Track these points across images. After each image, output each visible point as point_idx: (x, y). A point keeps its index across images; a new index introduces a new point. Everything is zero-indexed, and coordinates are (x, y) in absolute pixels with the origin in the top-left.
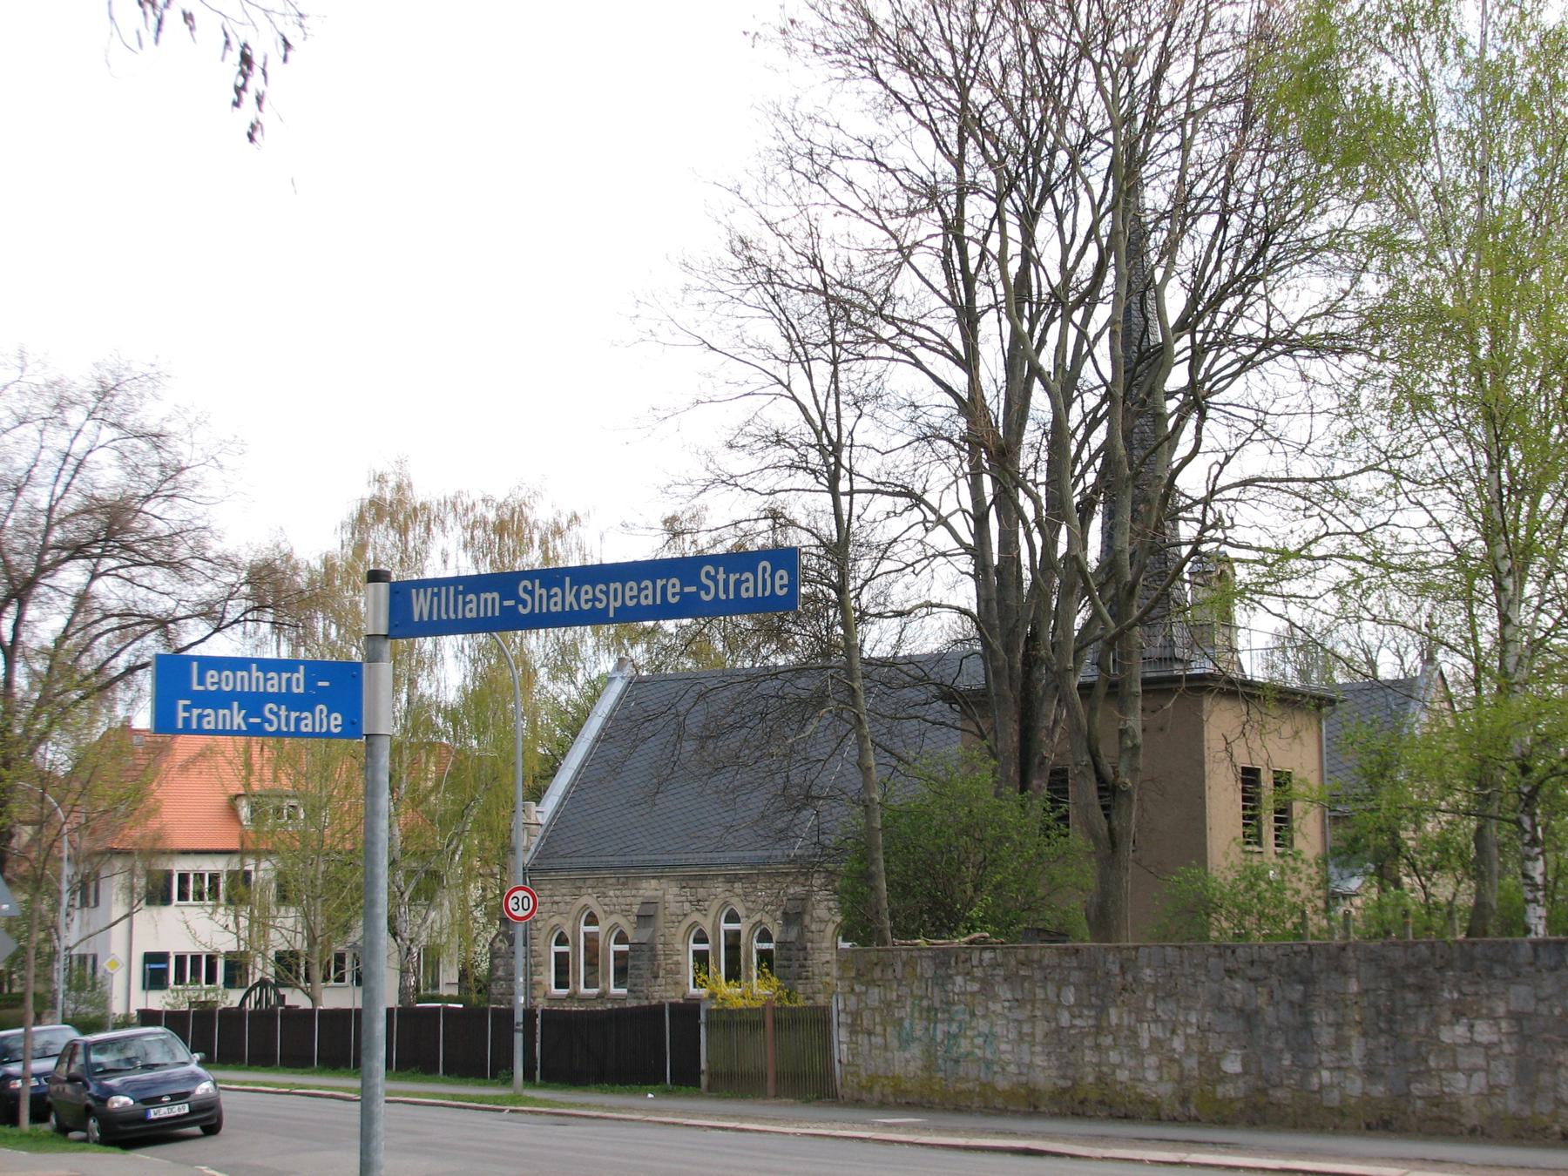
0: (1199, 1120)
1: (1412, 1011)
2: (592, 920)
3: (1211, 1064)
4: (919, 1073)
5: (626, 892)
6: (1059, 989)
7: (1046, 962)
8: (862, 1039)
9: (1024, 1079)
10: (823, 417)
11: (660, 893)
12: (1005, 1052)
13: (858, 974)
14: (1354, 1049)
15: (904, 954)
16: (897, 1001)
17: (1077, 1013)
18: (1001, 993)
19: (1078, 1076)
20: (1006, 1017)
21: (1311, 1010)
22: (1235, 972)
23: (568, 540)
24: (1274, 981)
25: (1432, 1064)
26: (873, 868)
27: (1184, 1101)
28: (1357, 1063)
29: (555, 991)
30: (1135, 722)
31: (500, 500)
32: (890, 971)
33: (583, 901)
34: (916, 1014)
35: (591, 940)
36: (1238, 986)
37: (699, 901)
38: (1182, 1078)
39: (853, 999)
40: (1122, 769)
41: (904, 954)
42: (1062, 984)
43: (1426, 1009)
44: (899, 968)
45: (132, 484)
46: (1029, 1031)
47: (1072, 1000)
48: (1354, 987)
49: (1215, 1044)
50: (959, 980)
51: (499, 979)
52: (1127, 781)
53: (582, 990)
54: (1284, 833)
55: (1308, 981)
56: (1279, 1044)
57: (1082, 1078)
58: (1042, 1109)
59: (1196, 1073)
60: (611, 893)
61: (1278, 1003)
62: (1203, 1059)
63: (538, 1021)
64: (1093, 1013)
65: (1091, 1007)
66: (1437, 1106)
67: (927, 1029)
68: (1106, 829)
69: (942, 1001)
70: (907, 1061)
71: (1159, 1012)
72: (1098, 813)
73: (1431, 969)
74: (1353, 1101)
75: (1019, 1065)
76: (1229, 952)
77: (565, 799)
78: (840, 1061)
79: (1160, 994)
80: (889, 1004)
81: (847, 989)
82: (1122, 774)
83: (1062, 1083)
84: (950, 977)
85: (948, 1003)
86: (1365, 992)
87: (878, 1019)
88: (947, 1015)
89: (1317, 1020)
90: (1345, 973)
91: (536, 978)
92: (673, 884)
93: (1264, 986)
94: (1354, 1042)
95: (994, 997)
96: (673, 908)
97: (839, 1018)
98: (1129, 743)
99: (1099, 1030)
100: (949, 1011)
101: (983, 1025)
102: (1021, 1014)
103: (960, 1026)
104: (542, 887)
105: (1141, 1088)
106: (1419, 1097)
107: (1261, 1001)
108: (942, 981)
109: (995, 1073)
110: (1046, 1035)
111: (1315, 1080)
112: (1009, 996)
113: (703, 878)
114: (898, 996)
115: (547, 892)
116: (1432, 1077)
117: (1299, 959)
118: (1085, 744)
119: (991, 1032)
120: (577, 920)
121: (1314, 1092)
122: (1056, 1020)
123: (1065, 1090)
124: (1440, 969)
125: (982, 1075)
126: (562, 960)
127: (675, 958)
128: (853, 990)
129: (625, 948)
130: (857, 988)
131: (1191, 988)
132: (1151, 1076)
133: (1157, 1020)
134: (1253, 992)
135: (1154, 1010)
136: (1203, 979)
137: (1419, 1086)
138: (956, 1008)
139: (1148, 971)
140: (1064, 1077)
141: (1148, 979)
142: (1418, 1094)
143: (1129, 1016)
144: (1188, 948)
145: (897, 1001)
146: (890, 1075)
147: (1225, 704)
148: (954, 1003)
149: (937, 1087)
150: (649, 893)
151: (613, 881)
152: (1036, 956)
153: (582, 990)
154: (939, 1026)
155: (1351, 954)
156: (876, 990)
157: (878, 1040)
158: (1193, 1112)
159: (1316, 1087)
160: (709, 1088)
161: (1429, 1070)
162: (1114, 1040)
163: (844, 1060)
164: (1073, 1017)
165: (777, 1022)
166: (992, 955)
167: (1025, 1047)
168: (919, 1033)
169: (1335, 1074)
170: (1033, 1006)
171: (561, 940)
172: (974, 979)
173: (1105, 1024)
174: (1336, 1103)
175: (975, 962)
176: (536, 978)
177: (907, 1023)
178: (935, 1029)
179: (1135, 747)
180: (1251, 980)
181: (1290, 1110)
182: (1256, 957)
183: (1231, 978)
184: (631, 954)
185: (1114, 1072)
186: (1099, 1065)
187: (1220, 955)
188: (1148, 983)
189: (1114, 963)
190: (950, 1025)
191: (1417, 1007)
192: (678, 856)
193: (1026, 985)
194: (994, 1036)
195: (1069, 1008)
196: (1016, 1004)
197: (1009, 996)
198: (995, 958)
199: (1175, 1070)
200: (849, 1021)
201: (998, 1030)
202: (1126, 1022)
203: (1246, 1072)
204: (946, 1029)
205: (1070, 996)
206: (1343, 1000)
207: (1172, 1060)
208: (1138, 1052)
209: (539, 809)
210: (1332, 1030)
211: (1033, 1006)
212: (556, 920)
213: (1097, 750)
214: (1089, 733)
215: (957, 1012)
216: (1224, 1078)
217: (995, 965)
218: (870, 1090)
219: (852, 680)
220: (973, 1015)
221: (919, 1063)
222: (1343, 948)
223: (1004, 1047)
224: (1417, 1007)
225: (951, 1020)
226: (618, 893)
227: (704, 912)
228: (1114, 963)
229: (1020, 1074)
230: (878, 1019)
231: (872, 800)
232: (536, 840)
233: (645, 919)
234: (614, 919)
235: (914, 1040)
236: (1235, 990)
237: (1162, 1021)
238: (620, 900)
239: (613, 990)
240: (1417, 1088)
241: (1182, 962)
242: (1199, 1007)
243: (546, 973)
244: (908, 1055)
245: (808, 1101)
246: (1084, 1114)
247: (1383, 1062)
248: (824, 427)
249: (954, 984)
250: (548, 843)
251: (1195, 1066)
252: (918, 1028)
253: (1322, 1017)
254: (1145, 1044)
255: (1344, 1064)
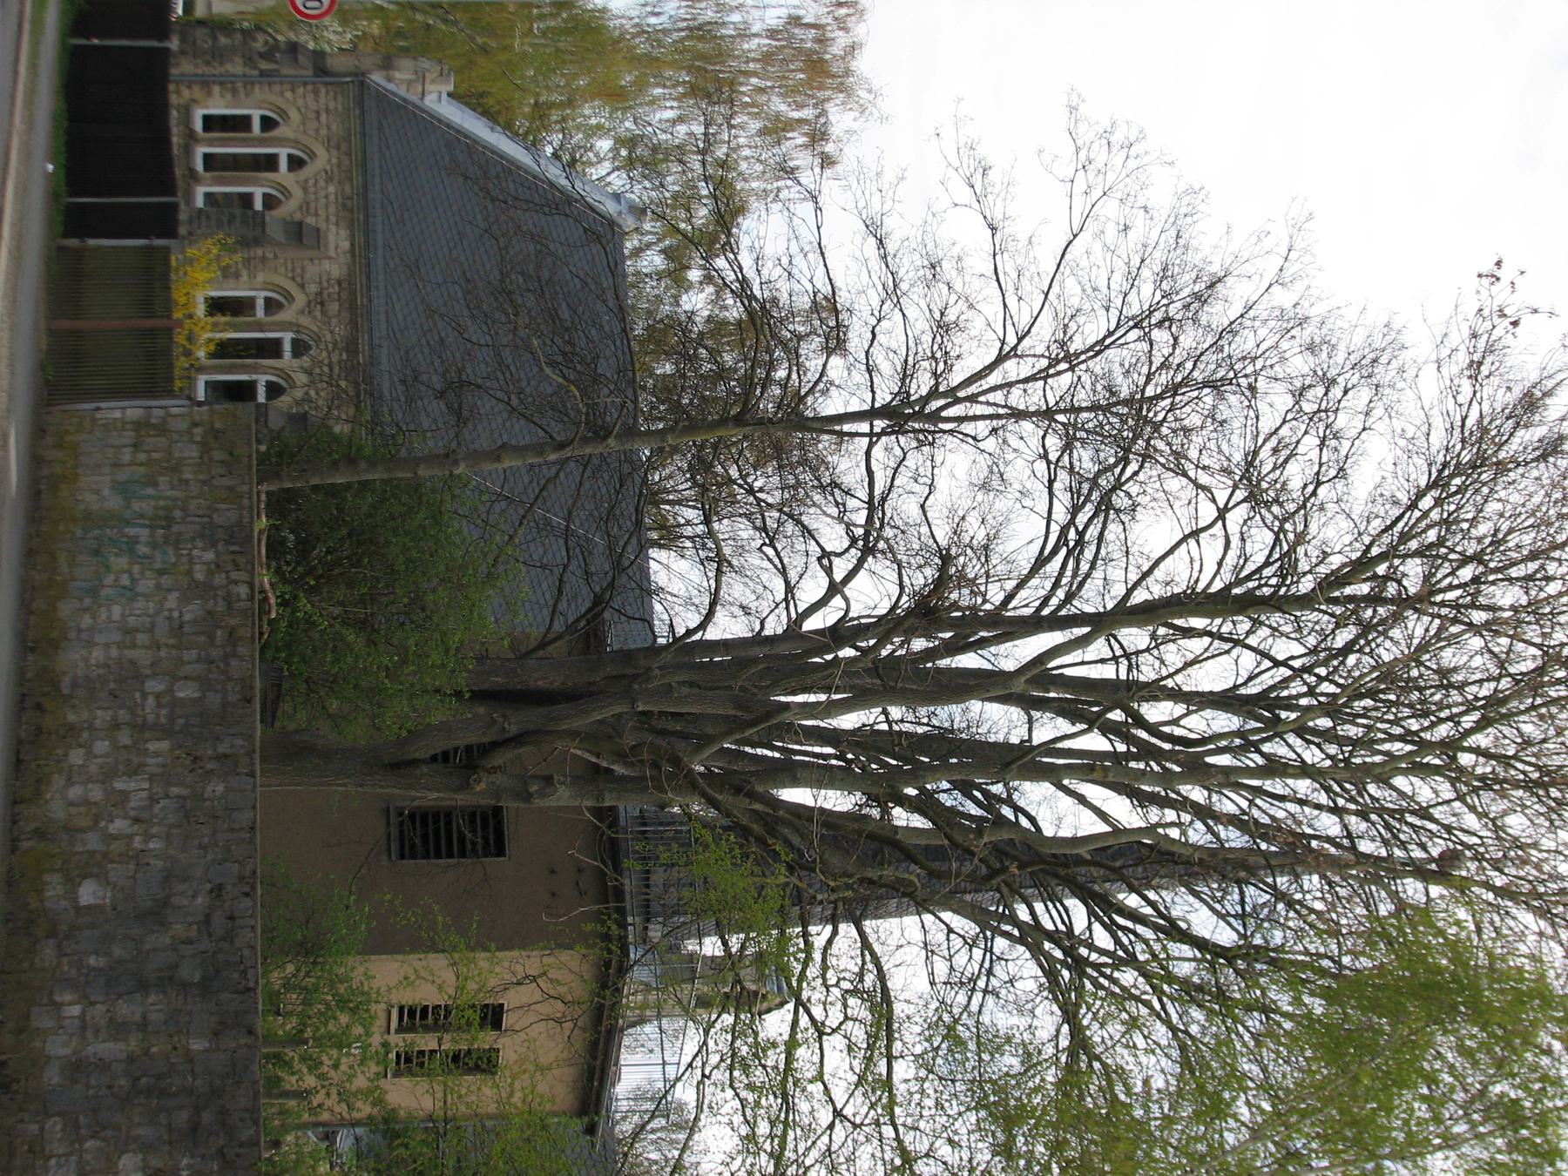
0: (13, 852)
1: (163, 1118)
2: (295, 163)
3: (93, 867)
4: (82, 506)
5: (332, 209)
6: (197, 679)
7: (234, 662)
8: (129, 436)
9: (72, 635)
10: (972, 399)
11: (332, 253)
12: (109, 611)
13: (218, 431)
14: (110, 1045)
15: (245, 488)
16: (180, 480)
17: (164, 701)
18: (191, 607)
19: (76, 701)
20: (157, 614)
21: (165, 992)
22: (218, 896)
23: (801, 155)
24: (206, 944)
25: (89, 1144)
26: (363, 465)
27: (40, 834)
28: (91, 1050)
29: (198, 114)
30: (562, 796)
31: (854, 65)
32: (221, 471)
33: (321, 151)
34: (162, 503)
35: (270, 163)
36: (199, 900)
37: (322, 304)
38: (70, 830)
39: (184, 425)
40: (500, 779)
41: (245, 488)
42: (204, 683)
43: (166, 1137)
44: (226, 482)
46: (139, 642)
47: (181, 695)
48: (197, 1045)
49: (118, 872)
50: (210, 556)
51: (215, 38)
52: (483, 785)
53: (201, 151)
54: (410, 1063)
55: (205, 987)
56: (118, 951)
57: (73, 707)
58: (30, 657)
59: (79, 848)
61: (175, 950)
62: (98, 857)
63: (155, 44)
64: (163, 720)
65: (172, 718)
66: (30, 1151)
67: (142, 516)
68: (417, 755)
69: (180, 534)
70: (97, 492)
71: (162, 803)
72: (440, 745)
73: (221, 1142)
74: (38, 1044)
75: (91, 629)
76: (246, 889)
77: (458, 131)
78: (98, 409)
79: (189, 804)
80: (176, 469)
81: (197, 418)
82: (492, 778)
83: (66, 683)
84: (213, 545)
85: (178, 542)
86: (189, 1058)
87: (155, 455)
88: (160, 540)
89: (152, 998)
90: (216, 1034)
91: (216, 89)
92: (345, 271)
93: (199, 931)
94: (121, 1045)
95: (185, 599)
96: (312, 270)
97: (158, 407)
98: (534, 788)
99: (140, 727)
100: (166, 542)
101: (147, 584)
102: (162, 630)
103: (147, 557)
104: (340, 99)
105: (58, 780)
106: (42, 1129)
107: (178, 929)
108: (208, 534)
109: (81, 600)
110: (132, 662)
111: (68, 997)
112: (187, 617)
113: (352, 308)
114: (187, 481)
116: (72, 1144)
117: (236, 976)
118: (532, 727)
119: (138, 594)
120: (296, 143)
121: (51, 994)
122: (154, 675)
123: (55, 685)
124: (221, 1153)
125: (78, 583)
126: (242, 123)
127: (245, 273)
128: (196, 425)
129: (258, 205)
130: (198, 431)
131: (196, 842)
132: (75, 792)
133: (153, 800)
134: (190, 919)
135: (167, 796)
136: (209, 857)
137: (58, 1128)
138: (171, 551)
139: (220, 788)
140: (75, 685)
141: (209, 789)
142: (47, 1126)
143: (158, 765)
144: (252, 839)
145: (180, 480)
146: (79, 471)
147: (587, 970)
148: (177, 548)
149: (61, 528)
150: (331, 238)
152: (242, 650)
153: (201, 151)
154: (145, 532)
155: (242, 1041)
156: (195, 454)
157: (126, 456)
158: (25, 845)
159: (57, 998)
160: (61, 249)
161: (81, 1140)
162: (125, 747)
163: (98, 415)
164: (158, 696)
165: (152, 333)
166: (243, 596)
167: (117, 637)
168: (137, 506)
169: (76, 1022)
170: (173, 646)
171: (268, 123)
172: (210, 573)
173: (147, 735)
174: (35, 1023)
175: (234, 575)
176: (216, 89)
177: (150, 491)
178: (143, 526)
179: (528, 797)
180: (208, 916)
181: (26, 965)
182: (239, 922)
183: (211, 891)
184: (250, 213)
185: (81, 746)
186: (91, 727)
187: (242, 878)
188: (204, 788)
189: (232, 746)
190: (147, 544)
191: (169, 1125)
192: (381, 277)
193: (203, 638)
194: (132, 599)
195: (170, 691)
196: (176, 624)
197: (187, 617)
198: (239, 600)
199: (84, 823)
200: (154, 421)
201: (140, 604)
202: (150, 761)
203: (79, 909)
204: (142, 539)
205: (186, 692)
206: (180, 1032)
207: (97, 818)
208: (107, 776)
209: (444, 96)
210: (138, 1018)
211: (173, 646)
212: (294, 115)
213: (522, 744)
214: (549, 733)
215: (165, 553)
216: (72, 884)
217: (229, 600)
218: (59, 446)
219: (618, 437)
220: (161, 572)
221: (95, 507)
222: (250, 1032)
223: (117, 611)
224: (169, 1125)
225: (154, 546)
226: (332, 198)
227: (308, 309)
228: (232, 746)
229: (80, 631)
230: (155, 455)
231: (456, 463)
232: (402, 92)
233: (298, 233)
234: (297, 193)
235: (127, 500)
236: (194, 897)
237: (151, 806)
238: (323, 201)
239: (200, 191)
240: (55, 1125)
241: (233, 830)
242: (171, 852)
244: (106, 492)
245: (43, 367)
246: (24, 709)
247: (93, 1082)
248: (958, 401)
249: (204, 550)
250: (398, 106)
251: (89, 847)
252: (144, 505)
253: (155, 1005)
254: (119, 785)
255: (89, 1034)
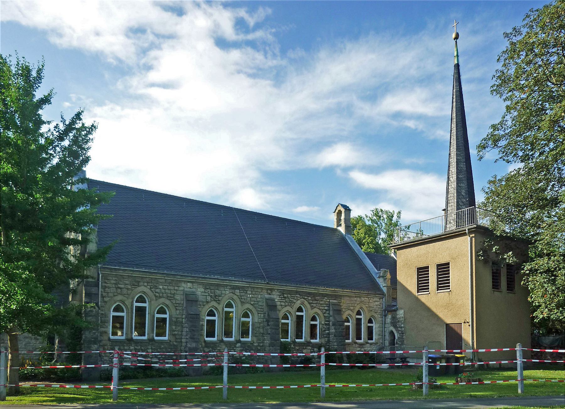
45: (296, 354)
60: (161, 287)
78: (6, 349)
115: (113, 282)
151: (163, 281)
226: (166, 287)
243: (107, 327)
